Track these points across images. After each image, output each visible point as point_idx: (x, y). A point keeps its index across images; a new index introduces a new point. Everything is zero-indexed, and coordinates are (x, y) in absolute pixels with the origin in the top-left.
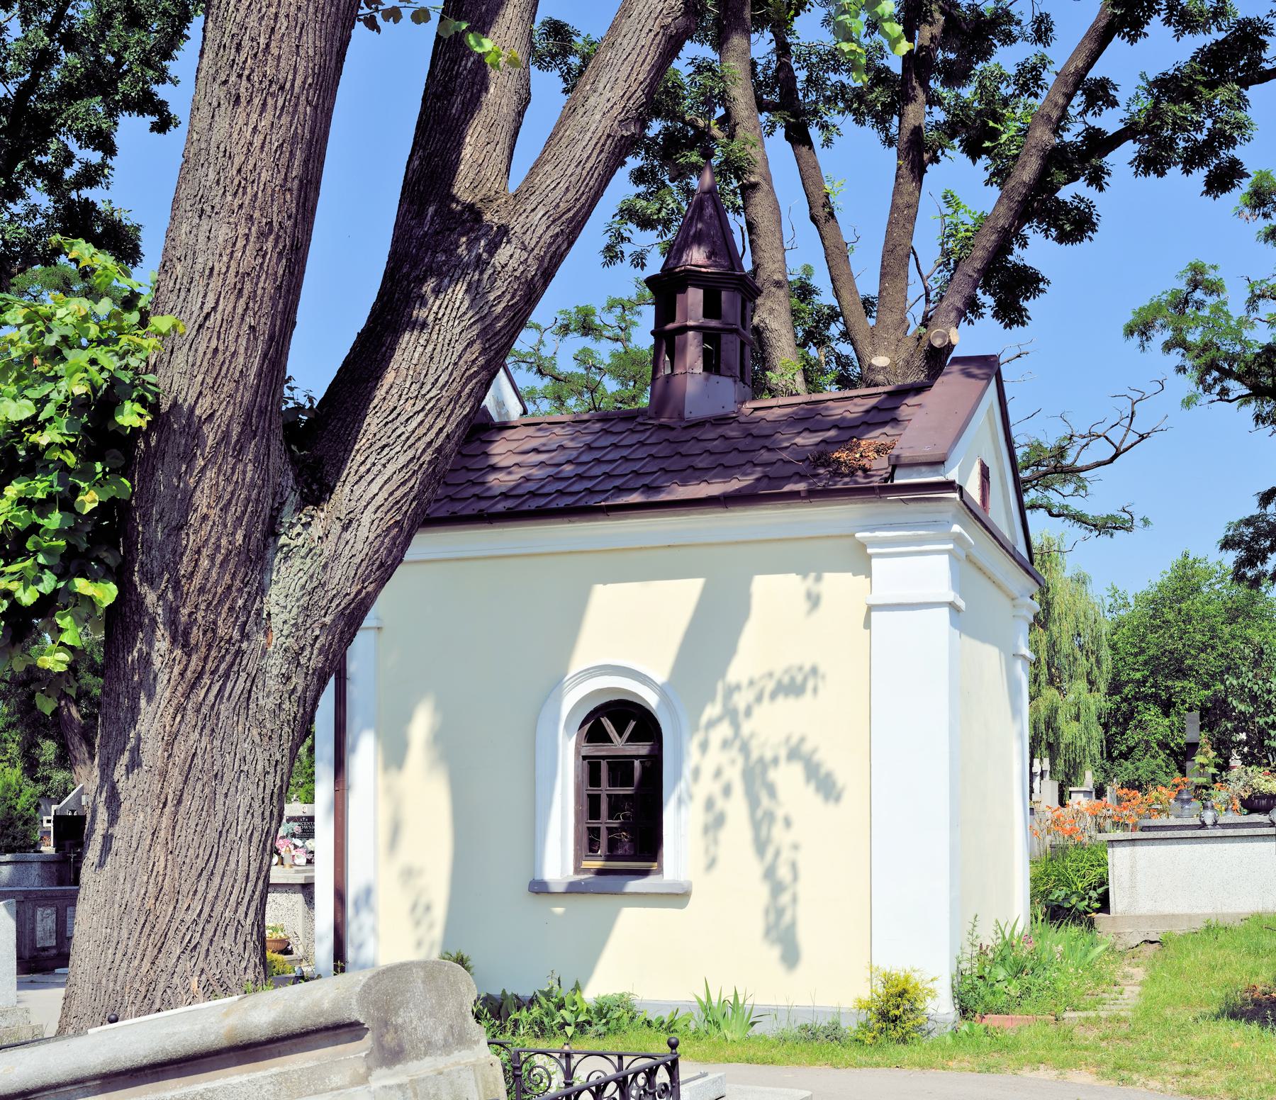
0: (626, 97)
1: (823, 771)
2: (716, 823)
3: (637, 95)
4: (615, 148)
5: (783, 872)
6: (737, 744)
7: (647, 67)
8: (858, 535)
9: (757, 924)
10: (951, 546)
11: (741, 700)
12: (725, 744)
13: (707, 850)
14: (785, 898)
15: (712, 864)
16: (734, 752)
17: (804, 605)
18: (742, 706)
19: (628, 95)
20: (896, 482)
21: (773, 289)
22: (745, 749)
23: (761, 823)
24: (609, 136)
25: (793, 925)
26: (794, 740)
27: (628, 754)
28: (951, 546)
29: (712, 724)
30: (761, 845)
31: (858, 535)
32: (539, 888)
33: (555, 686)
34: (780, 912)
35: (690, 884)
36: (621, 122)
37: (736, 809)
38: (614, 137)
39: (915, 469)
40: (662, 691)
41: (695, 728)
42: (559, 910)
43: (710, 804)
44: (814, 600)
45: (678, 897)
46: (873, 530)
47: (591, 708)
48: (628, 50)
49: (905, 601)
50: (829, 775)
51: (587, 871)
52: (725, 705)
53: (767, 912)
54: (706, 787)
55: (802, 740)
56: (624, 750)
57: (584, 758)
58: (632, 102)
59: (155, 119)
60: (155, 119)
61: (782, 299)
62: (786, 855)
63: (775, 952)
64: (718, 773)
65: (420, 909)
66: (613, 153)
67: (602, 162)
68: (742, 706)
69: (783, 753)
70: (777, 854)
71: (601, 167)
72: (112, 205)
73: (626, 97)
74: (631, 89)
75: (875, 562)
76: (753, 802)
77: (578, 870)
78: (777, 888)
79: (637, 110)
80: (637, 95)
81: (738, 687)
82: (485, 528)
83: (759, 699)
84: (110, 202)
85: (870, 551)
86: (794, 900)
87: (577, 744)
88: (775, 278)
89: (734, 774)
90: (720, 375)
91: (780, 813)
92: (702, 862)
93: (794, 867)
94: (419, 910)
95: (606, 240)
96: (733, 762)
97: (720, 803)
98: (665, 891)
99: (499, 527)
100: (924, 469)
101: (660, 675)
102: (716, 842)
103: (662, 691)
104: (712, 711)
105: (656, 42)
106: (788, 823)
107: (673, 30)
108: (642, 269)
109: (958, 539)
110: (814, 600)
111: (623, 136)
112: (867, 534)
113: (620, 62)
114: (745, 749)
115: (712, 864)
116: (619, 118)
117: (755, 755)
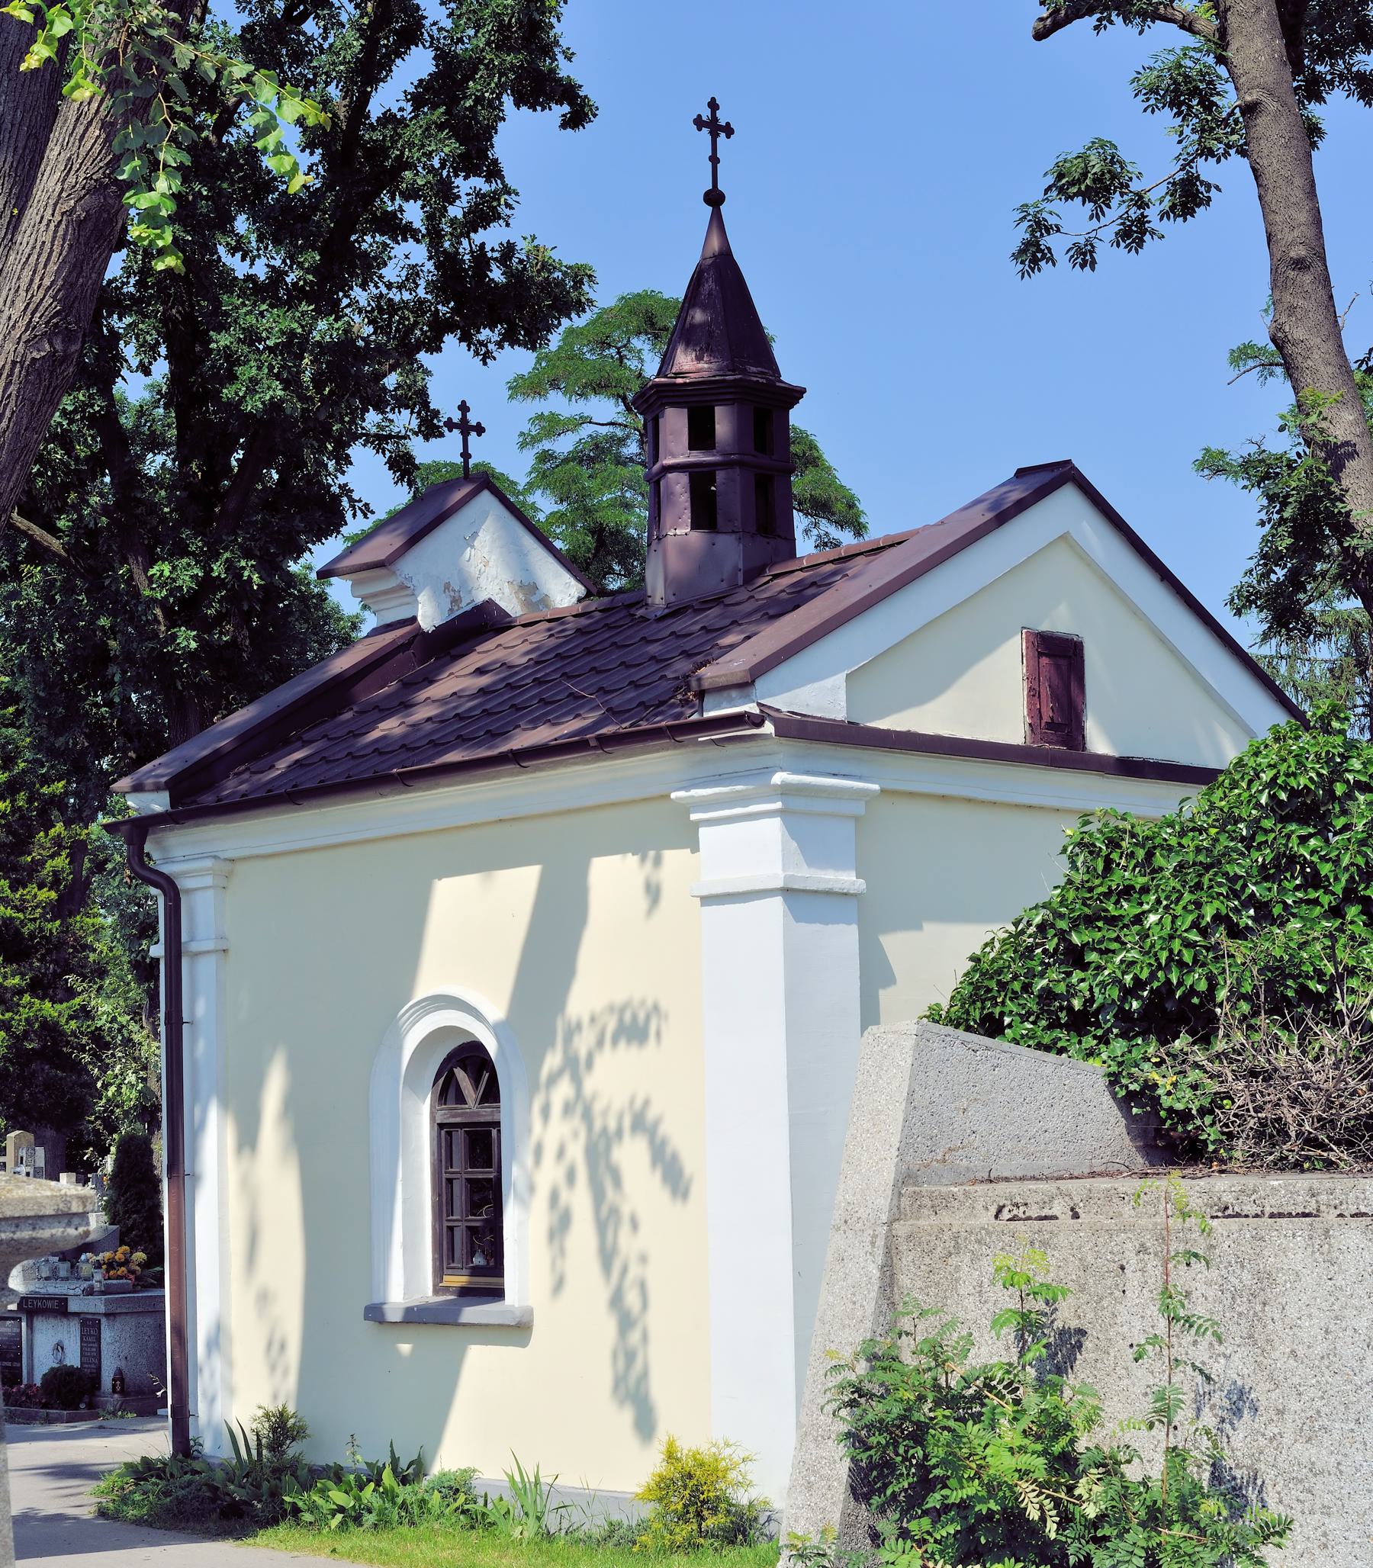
0: (29, 312)
1: (669, 1150)
2: (560, 1226)
3: (45, 304)
4: (28, 374)
5: (632, 1299)
6: (579, 1109)
7: (53, 267)
8: (673, 795)
9: (604, 1377)
10: (778, 805)
11: (583, 1043)
12: (568, 1109)
13: (553, 1264)
14: (635, 1337)
15: (559, 1285)
16: (576, 1121)
17: (642, 902)
18: (583, 1054)
19: (32, 306)
20: (708, 715)
21: (1292, 274)
22: (587, 1116)
23: (606, 1221)
24: (14, 363)
25: (645, 1376)
26: (639, 1103)
27: (482, 1120)
28: (778, 805)
29: (553, 1079)
30: (607, 1256)
31: (673, 795)
32: (375, 1313)
33: (390, 1032)
34: (630, 1357)
35: (530, 1312)
36: (26, 342)
37: (580, 1201)
38: (22, 363)
39: (725, 694)
40: (497, 1029)
41: (533, 1087)
42: (405, 1348)
43: (554, 1198)
44: (653, 893)
45: (518, 1331)
46: (687, 788)
47: (445, 1056)
48: (27, 251)
49: (731, 890)
50: (675, 1158)
51: (446, 1290)
52: (566, 1052)
53: (615, 1356)
54: (549, 1174)
55: (647, 1103)
56: (478, 1114)
57: (441, 1126)
58: (38, 315)
59: (566, 108)
60: (566, 108)
61: (1309, 288)
62: (634, 1272)
63: (626, 1417)
64: (561, 1153)
65: (276, 1347)
66: (27, 381)
67: (13, 397)
68: (583, 1054)
69: (627, 1122)
70: (624, 1270)
71: (12, 403)
72: (536, 243)
73: (29, 312)
74: (36, 299)
75: (703, 832)
76: (598, 1195)
77: (437, 1290)
78: (626, 1322)
79: (47, 323)
80: (45, 304)
81: (579, 1026)
82: (285, 812)
83: (600, 1043)
84: (534, 238)
85: (694, 817)
86: (645, 1338)
87: (432, 1107)
88: (1293, 254)
89: (576, 1152)
90: (718, 532)
91: (626, 1211)
92: (547, 1283)
93: (643, 1287)
94: (275, 1347)
95: (1022, 233)
96: (575, 1134)
97: (564, 1196)
98: (496, 1322)
99: (311, 808)
100: (734, 693)
101: (496, 1009)
102: (562, 1251)
103: (497, 1029)
104: (553, 1060)
105: (61, 232)
106: (635, 1225)
107: (80, 213)
108: (1093, 269)
109: (786, 791)
110: (653, 893)
111: (34, 360)
112: (682, 794)
113: (19, 267)
114: (587, 1116)
115: (559, 1285)
116: (25, 338)
117: (598, 1125)
